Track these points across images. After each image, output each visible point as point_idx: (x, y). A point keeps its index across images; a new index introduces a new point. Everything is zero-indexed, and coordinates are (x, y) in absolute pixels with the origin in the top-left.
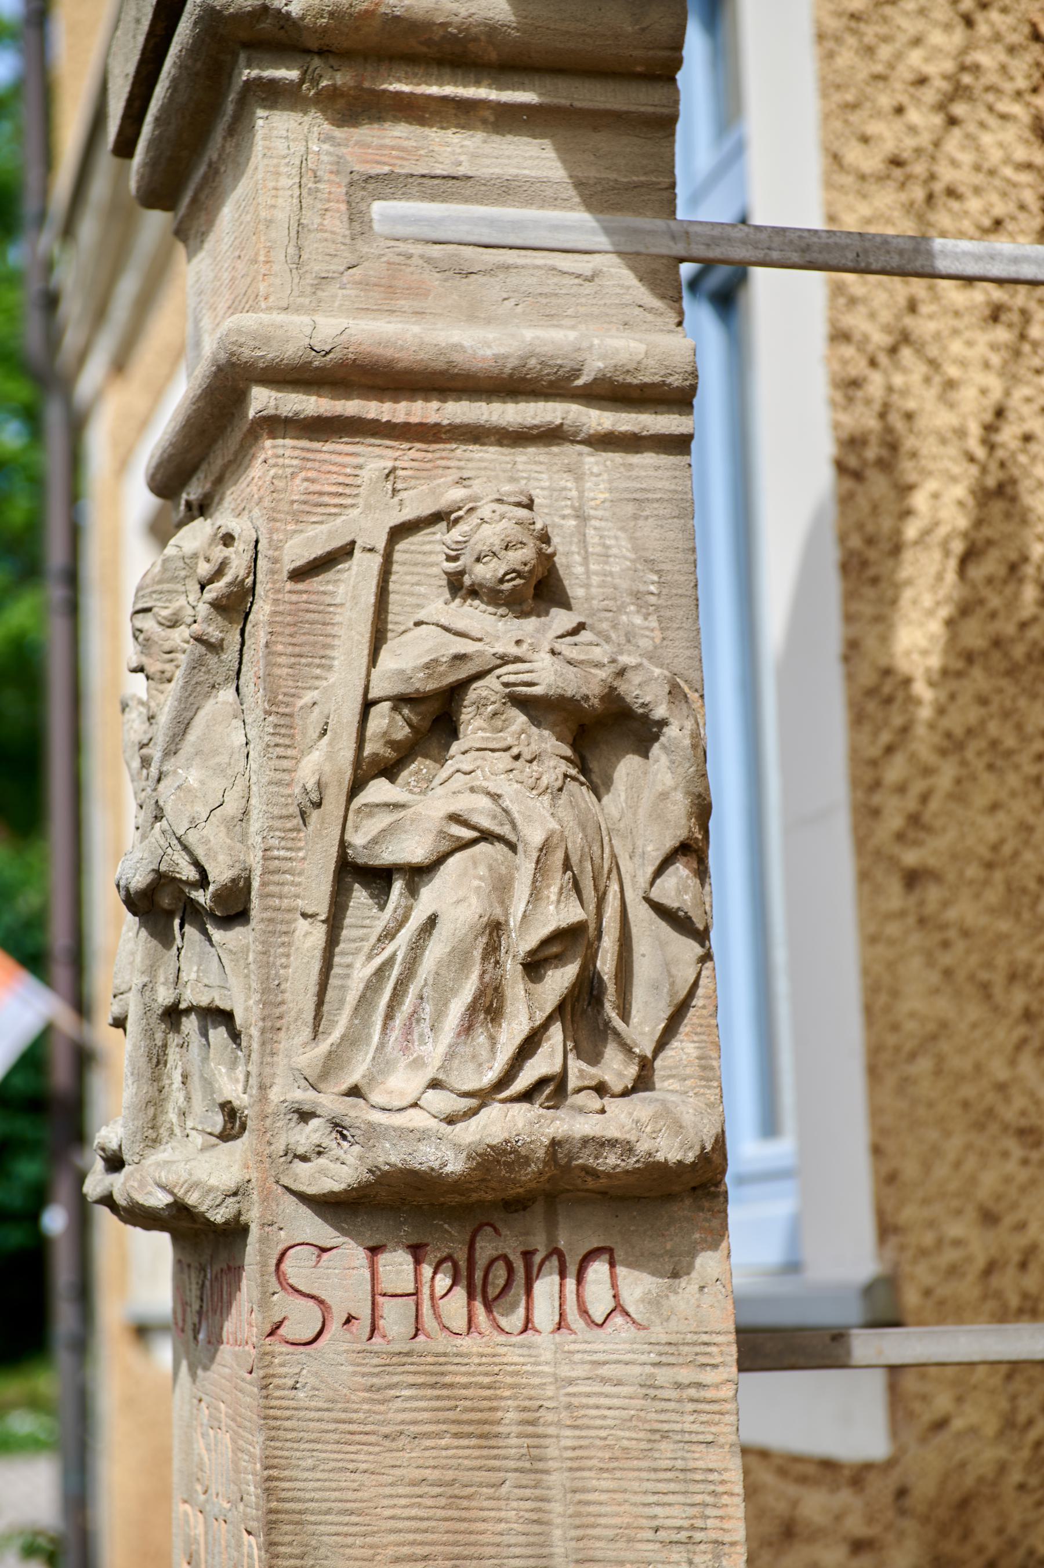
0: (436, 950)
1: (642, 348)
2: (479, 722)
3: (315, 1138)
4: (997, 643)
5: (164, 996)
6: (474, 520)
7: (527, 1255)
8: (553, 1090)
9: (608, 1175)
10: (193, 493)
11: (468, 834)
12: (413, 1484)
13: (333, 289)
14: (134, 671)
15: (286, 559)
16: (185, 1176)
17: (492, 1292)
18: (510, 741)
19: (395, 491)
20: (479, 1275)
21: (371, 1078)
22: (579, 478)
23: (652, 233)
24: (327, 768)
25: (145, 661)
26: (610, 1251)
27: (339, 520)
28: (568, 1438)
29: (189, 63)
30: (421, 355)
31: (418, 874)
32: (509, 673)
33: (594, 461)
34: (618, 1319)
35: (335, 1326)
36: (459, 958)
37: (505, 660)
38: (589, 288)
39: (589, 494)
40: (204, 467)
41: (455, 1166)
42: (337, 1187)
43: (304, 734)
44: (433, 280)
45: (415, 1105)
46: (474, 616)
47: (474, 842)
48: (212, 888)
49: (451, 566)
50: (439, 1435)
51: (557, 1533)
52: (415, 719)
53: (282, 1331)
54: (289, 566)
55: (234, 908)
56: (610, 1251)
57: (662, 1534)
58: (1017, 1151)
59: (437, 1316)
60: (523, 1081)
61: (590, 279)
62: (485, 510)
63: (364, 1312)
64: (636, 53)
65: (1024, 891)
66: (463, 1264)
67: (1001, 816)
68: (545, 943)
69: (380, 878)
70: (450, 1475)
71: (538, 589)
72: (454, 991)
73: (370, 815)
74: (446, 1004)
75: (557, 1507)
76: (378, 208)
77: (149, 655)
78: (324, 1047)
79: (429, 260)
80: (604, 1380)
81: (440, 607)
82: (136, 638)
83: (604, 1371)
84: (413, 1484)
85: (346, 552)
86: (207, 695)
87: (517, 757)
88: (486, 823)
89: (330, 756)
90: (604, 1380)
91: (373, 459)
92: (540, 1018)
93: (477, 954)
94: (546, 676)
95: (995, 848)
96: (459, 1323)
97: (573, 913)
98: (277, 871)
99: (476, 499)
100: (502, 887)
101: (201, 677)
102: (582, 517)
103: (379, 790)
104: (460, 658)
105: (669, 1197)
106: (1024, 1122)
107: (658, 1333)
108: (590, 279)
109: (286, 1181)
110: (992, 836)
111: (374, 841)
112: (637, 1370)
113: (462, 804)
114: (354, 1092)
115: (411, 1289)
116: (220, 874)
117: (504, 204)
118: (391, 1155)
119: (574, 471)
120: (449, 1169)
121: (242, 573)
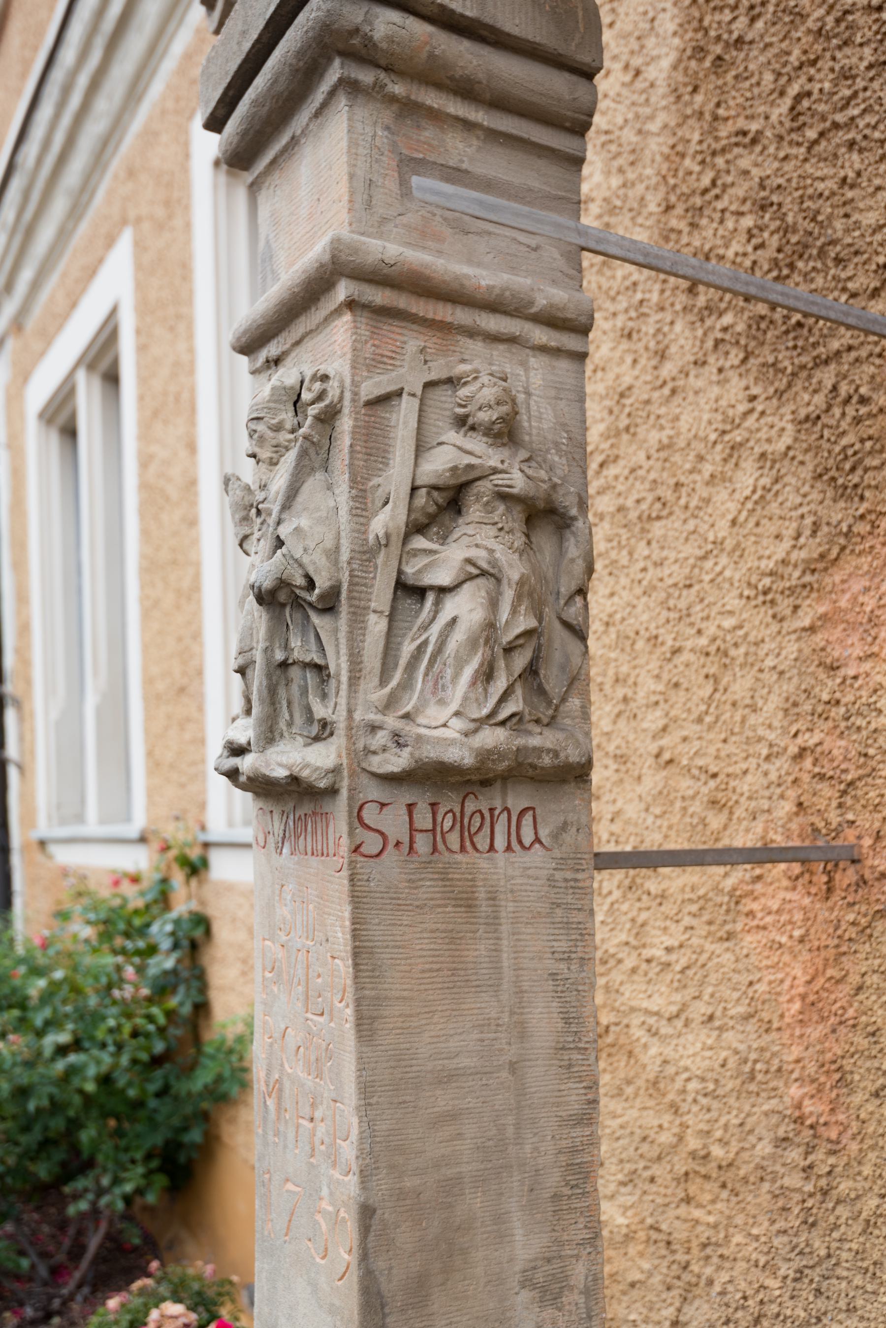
0: (458, 636)
1: (566, 296)
2: (477, 506)
3: (383, 742)
4: (620, 509)
5: (279, 656)
6: (478, 384)
7: (492, 810)
8: (514, 721)
9: (542, 768)
10: (272, 349)
11: (475, 571)
12: (432, 931)
13: (390, 226)
14: (249, 456)
15: (363, 393)
16: (299, 760)
17: (473, 830)
18: (496, 519)
19: (426, 362)
20: (466, 821)
21: (418, 710)
22: (527, 370)
23: (568, 228)
24: (391, 525)
25: (257, 450)
26: (533, 809)
27: (394, 374)
28: (511, 906)
29: (294, 61)
30: (447, 278)
31: (443, 591)
32: (498, 479)
33: (534, 361)
34: (537, 846)
35: (390, 847)
36: (472, 644)
37: (495, 471)
38: (534, 255)
39: (532, 380)
40: (284, 334)
41: (468, 760)
42: (396, 770)
43: (373, 502)
44: (447, 231)
45: (445, 725)
46: (477, 444)
47: (477, 576)
48: (317, 591)
49: (460, 411)
50: (446, 906)
51: (505, 955)
52: (440, 501)
53: (362, 849)
54: (364, 398)
55: (329, 605)
56: (533, 809)
57: (556, 955)
58: (614, 766)
59: (444, 842)
60: (503, 715)
61: (535, 249)
62: (485, 379)
63: (406, 840)
64: (569, 113)
65: (627, 637)
66: (458, 815)
67: (616, 599)
68: (518, 637)
69: (420, 592)
70: (451, 927)
71: (506, 432)
72: (467, 662)
73: (415, 556)
74: (461, 669)
75: (505, 942)
76: (415, 180)
77: (261, 447)
78: (387, 690)
79: (445, 219)
80: (529, 877)
81: (453, 436)
82: (251, 436)
83: (529, 872)
84: (432, 931)
85: (399, 393)
86: (309, 475)
87: (501, 529)
88: (485, 565)
89: (393, 517)
90: (529, 877)
91: (413, 341)
92: (511, 679)
93: (482, 641)
94: (517, 482)
95: (610, 616)
96: (456, 846)
97: (532, 623)
98: (357, 584)
99: (477, 371)
100: (494, 604)
101: (306, 462)
102: (528, 394)
103: (420, 542)
104: (470, 467)
105: (564, 781)
106: (618, 752)
107: (557, 853)
108: (535, 249)
109: (364, 765)
110: (609, 610)
111: (419, 571)
112: (546, 872)
113: (472, 553)
114: (407, 716)
115: (430, 827)
116: (322, 583)
117: (487, 193)
118: (431, 753)
119: (524, 364)
120: (466, 761)
121: (336, 400)
